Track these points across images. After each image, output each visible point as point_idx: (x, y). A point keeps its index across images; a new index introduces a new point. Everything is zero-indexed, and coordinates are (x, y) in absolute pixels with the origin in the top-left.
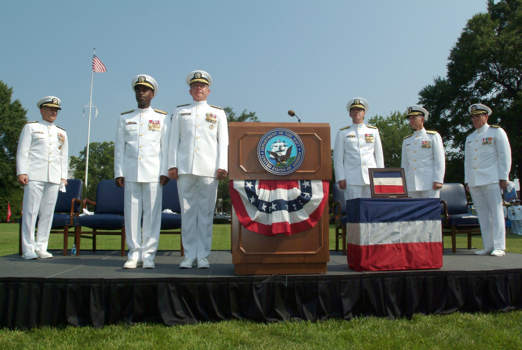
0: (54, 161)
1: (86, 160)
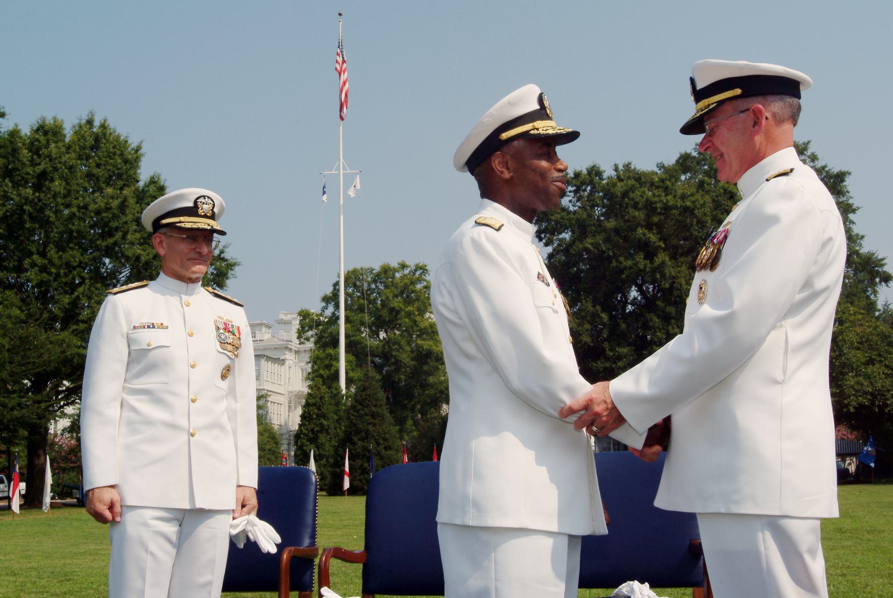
0: (209, 427)
1: (338, 318)
